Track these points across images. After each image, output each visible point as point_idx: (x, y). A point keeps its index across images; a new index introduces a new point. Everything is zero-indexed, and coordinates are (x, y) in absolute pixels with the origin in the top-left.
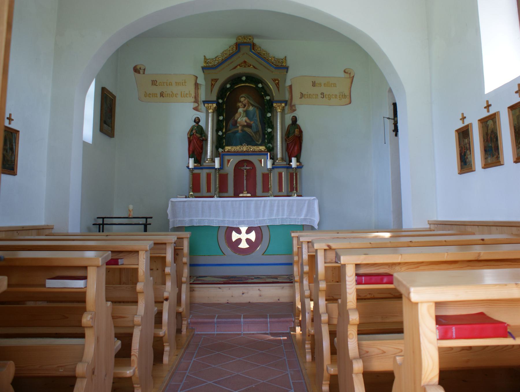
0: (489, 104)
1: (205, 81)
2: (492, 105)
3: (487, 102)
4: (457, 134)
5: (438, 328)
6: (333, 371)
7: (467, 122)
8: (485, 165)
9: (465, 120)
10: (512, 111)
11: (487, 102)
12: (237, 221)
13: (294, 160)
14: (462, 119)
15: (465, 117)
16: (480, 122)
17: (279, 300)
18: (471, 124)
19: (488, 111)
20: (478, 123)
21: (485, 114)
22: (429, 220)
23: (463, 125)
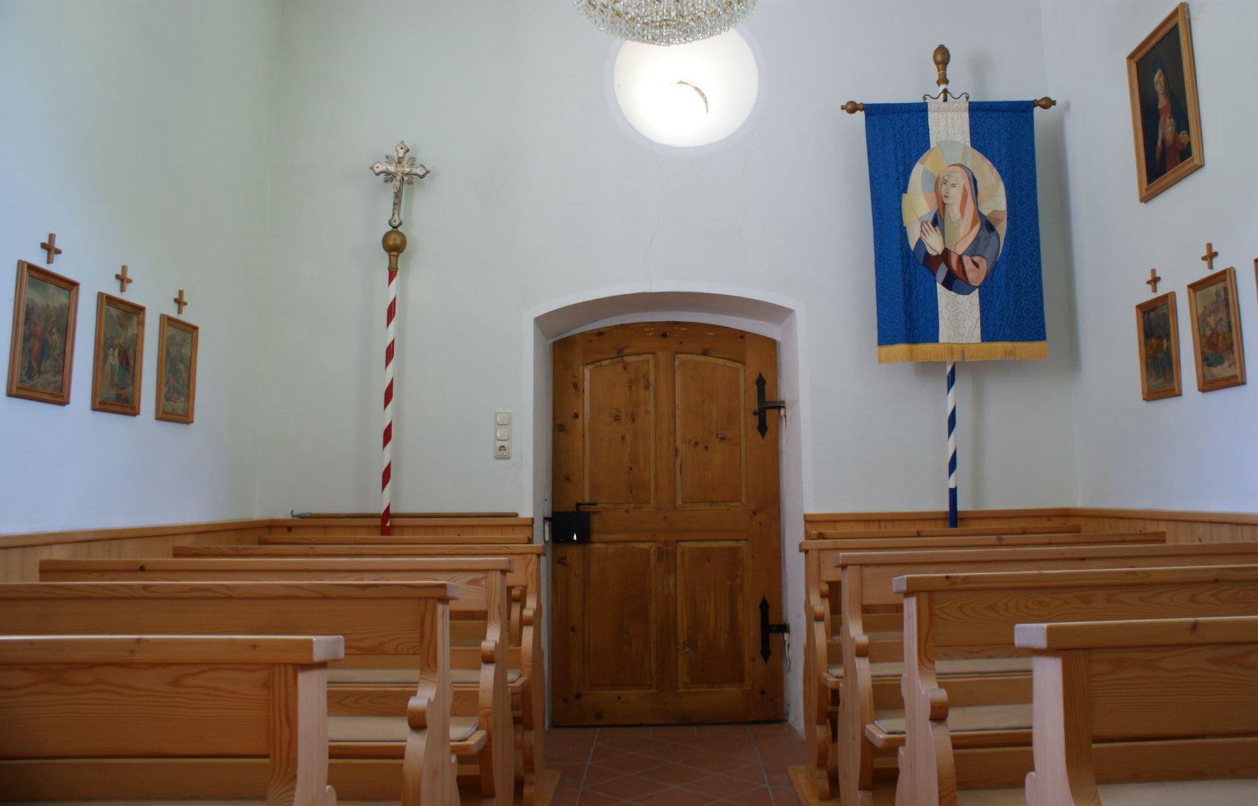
0: (1158, 275)
1: (901, 696)
2: (1162, 278)
3: (1153, 271)
4: (1141, 314)
5: (179, 406)
6: (531, 736)
7: (1162, 290)
8: (1204, 383)
9: (1215, 260)
10: (1195, 292)
11: (1153, 271)
12: (1166, 312)
13: (111, 350)
14: (1153, 283)
15: (1216, 254)
16: (1139, 310)
17: (546, 500)
18: (1173, 294)
19: (1155, 290)
20: (1137, 311)
21: (1147, 295)
22: (798, 550)
23: (1153, 296)
